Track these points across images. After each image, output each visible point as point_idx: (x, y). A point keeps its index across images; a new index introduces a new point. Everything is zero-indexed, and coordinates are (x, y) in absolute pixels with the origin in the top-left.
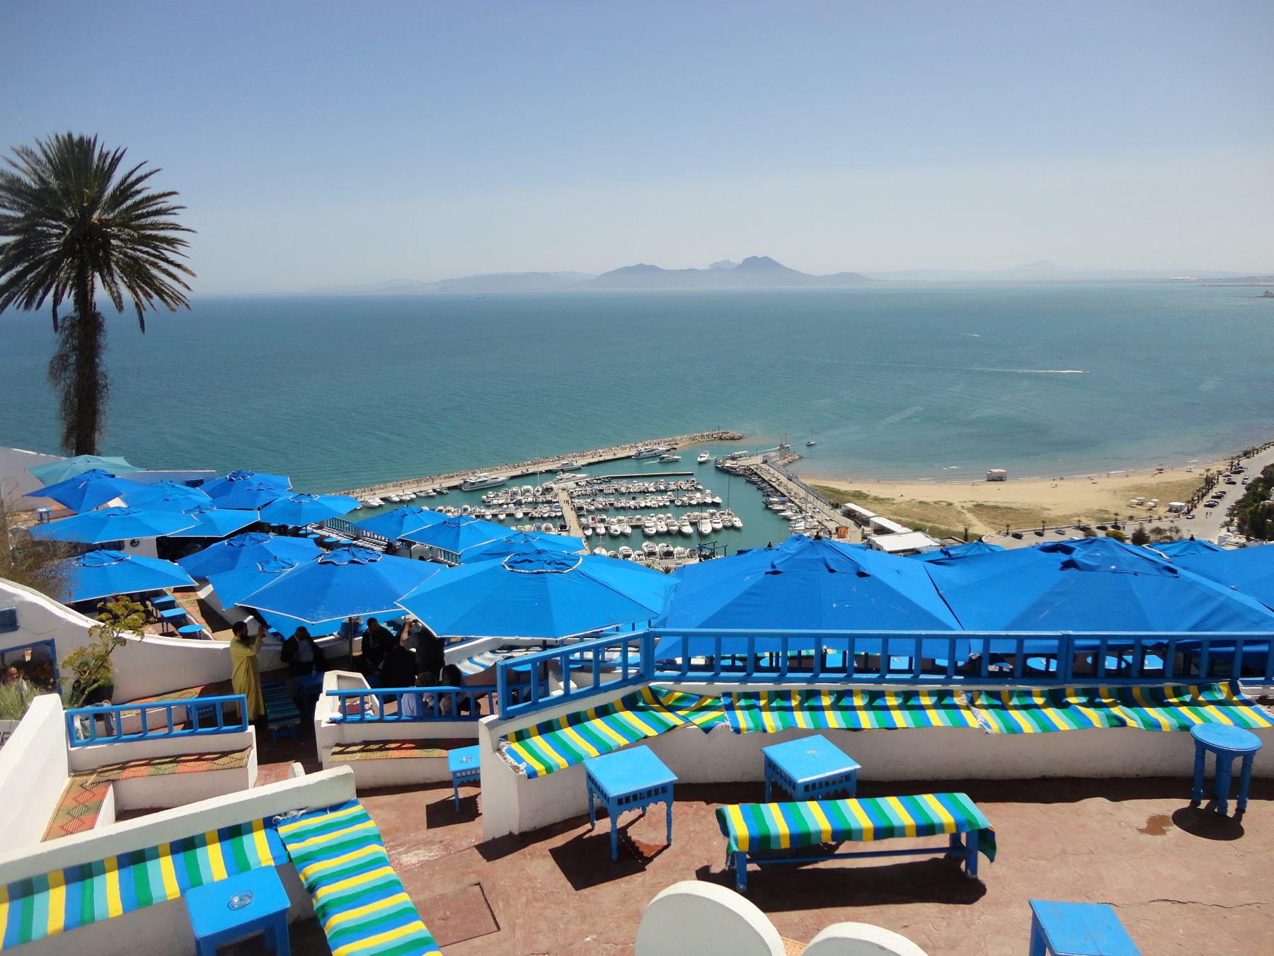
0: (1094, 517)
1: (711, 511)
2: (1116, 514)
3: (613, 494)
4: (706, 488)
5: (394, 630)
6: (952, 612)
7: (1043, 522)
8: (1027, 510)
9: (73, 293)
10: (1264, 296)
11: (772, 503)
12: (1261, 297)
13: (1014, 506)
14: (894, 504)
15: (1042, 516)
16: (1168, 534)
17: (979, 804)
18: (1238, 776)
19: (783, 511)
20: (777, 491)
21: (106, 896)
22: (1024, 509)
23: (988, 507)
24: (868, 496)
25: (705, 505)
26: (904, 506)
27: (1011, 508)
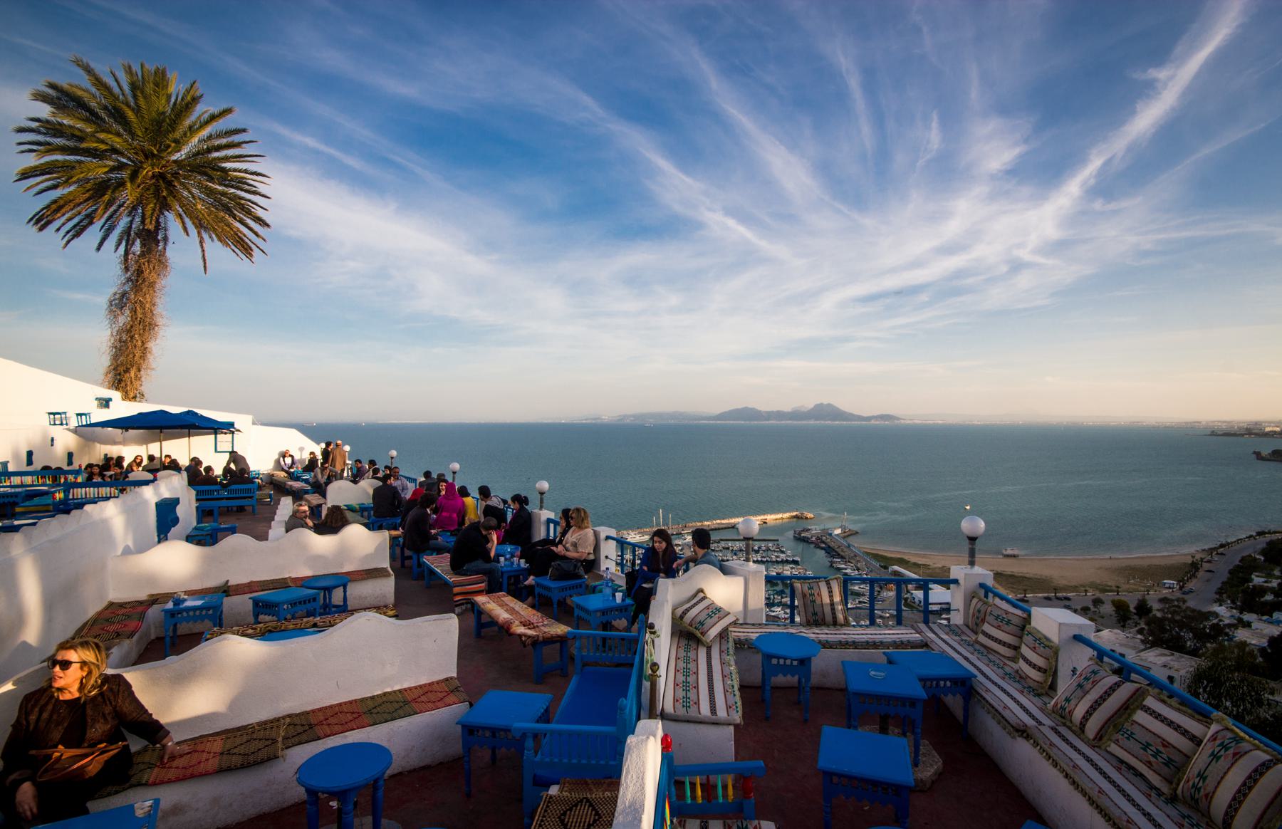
0: (1097, 588)
1: (791, 566)
2: (1118, 587)
3: (721, 551)
4: (788, 549)
5: (793, 676)
6: (715, 624)
7: (1055, 589)
8: (1039, 579)
9: (333, 59)
10: (1211, 435)
11: (834, 562)
12: (1209, 435)
13: (1027, 576)
14: (929, 569)
15: (1053, 584)
16: (1176, 603)
17: (20, 530)
18: (761, 685)
19: (846, 569)
20: (839, 555)
21: (93, 384)
22: (1036, 579)
23: (1005, 575)
24: (909, 562)
25: (787, 562)
26: (937, 571)
27: (1026, 578)
